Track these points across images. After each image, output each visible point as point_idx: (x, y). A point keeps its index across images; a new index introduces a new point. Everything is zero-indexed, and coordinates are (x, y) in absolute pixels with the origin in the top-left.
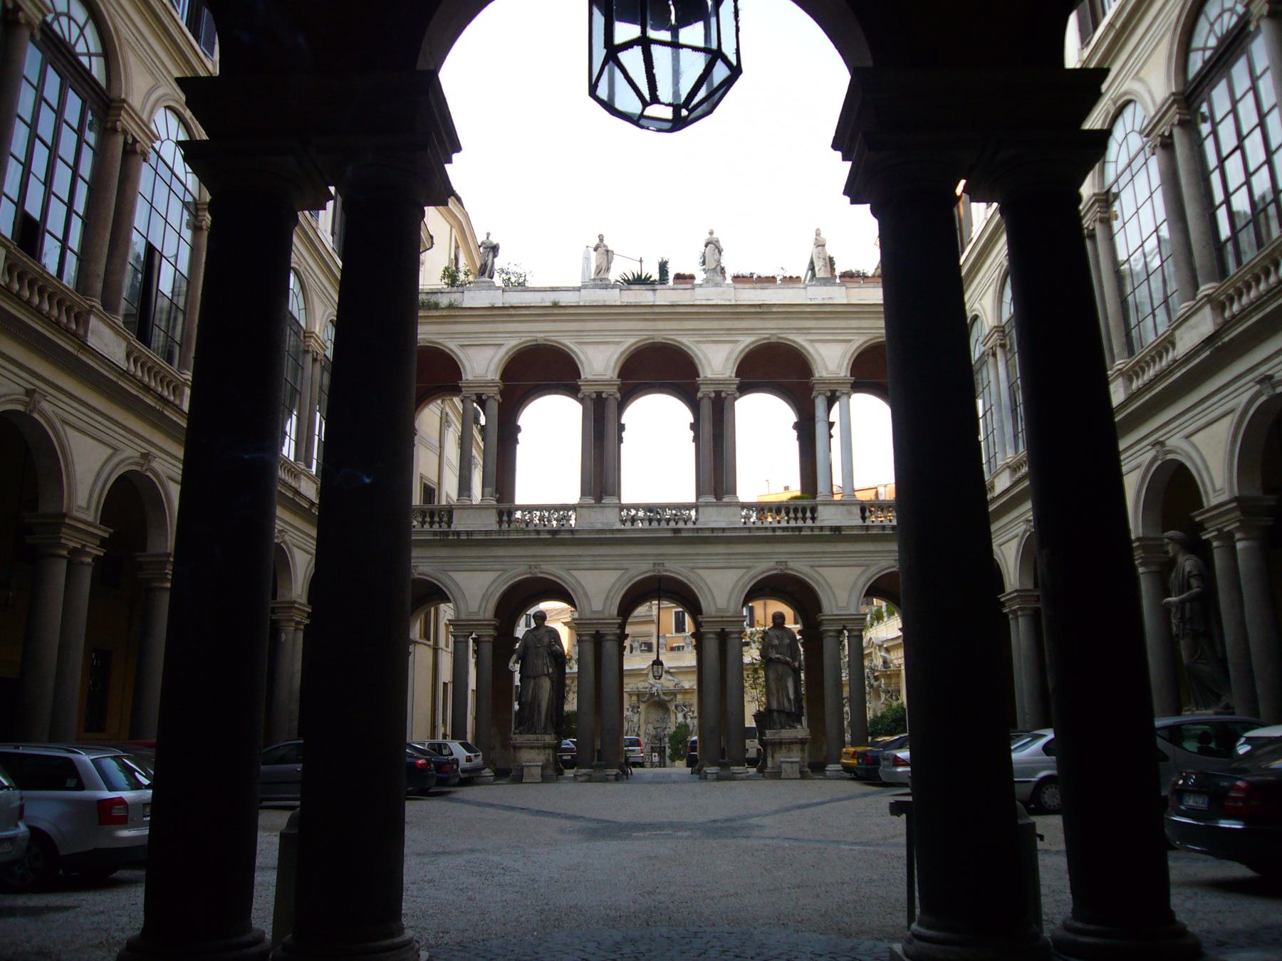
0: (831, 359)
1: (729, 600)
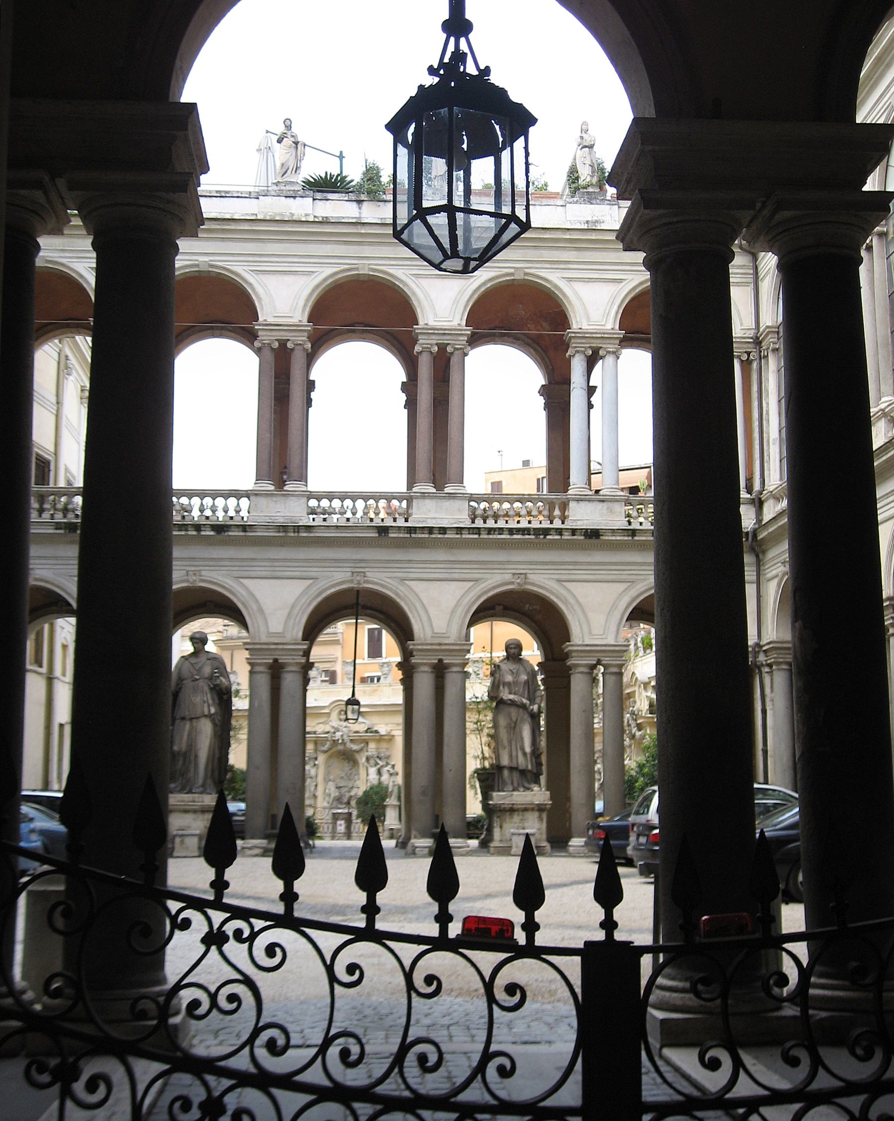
1: (450, 620)
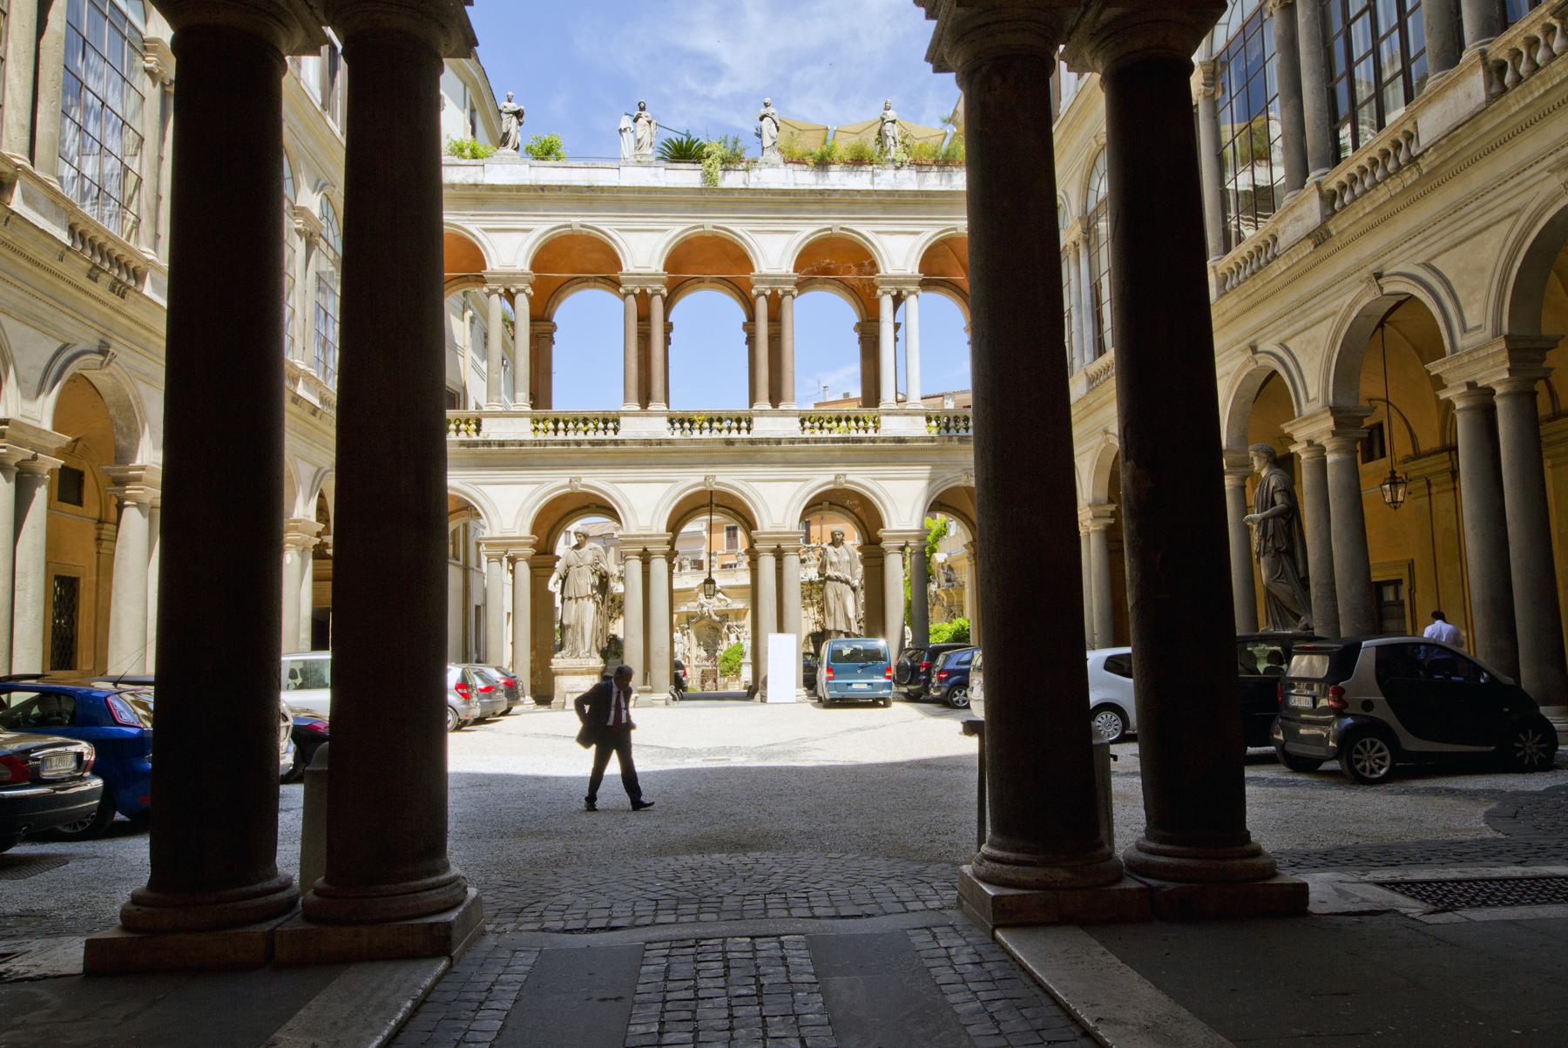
0: (899, 250)
